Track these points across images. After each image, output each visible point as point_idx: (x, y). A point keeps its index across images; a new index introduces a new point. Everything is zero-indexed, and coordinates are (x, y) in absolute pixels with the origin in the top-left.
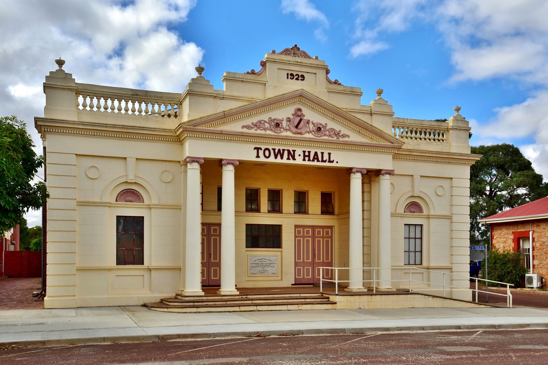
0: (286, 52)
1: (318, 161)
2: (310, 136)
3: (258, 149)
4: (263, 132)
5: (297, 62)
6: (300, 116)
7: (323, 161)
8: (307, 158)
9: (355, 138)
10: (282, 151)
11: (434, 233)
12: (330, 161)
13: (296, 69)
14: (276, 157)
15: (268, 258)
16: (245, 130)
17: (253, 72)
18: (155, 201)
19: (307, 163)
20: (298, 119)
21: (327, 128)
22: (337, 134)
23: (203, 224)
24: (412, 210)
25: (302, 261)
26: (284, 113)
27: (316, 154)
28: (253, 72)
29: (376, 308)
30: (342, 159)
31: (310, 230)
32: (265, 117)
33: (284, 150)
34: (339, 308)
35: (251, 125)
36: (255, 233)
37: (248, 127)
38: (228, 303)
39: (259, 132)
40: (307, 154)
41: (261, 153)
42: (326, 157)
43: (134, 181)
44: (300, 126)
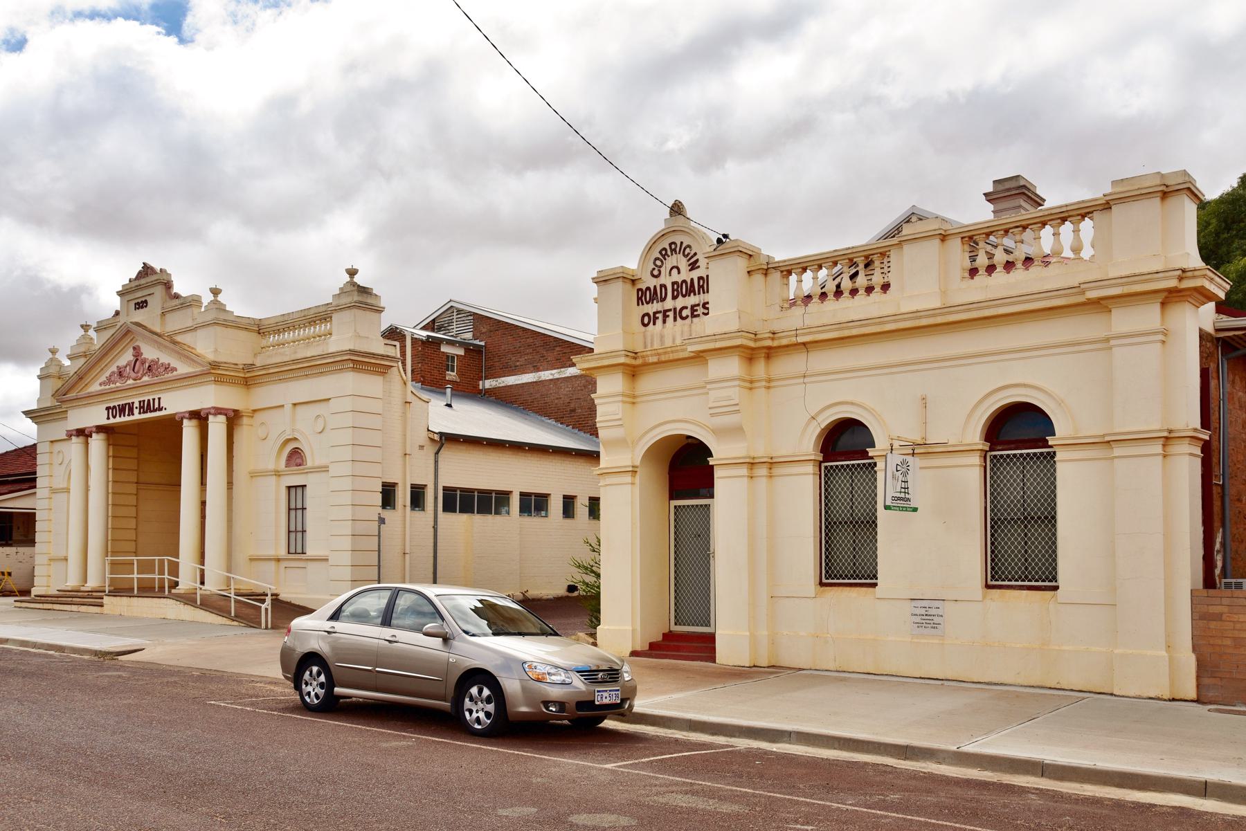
30: (175, 403)
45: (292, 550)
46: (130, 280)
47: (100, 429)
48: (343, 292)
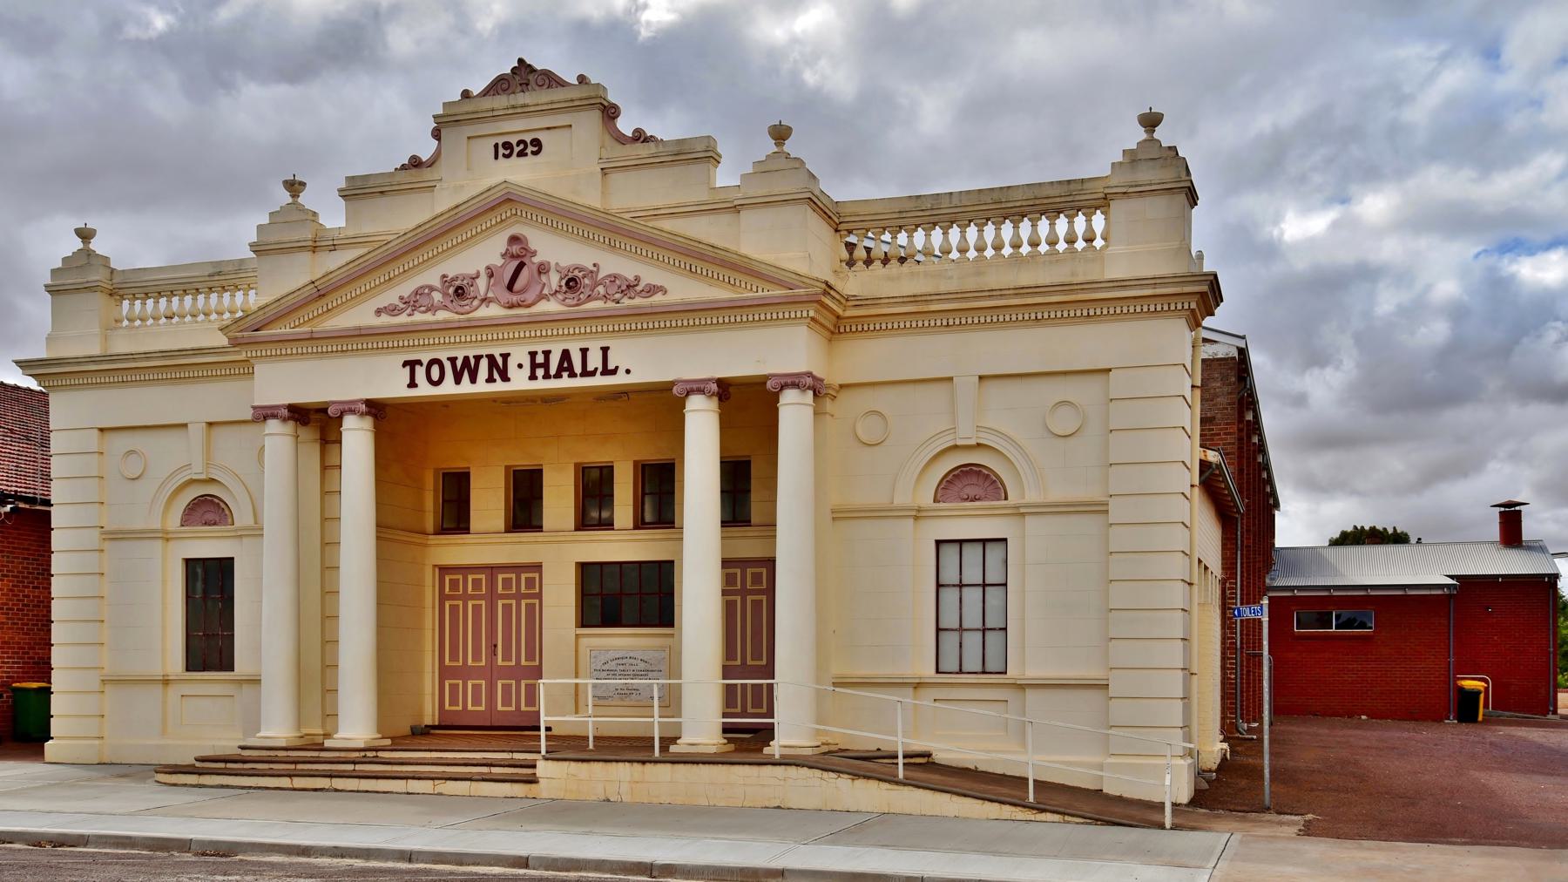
0: (499, 85)
1: (572, 375)
2: (551, 307)
3: (412, 365)
4: (428, 317)
5: (514, 107)
6: (518, 256)
7: (586, 373)
8: (540, 372)
9: (682, 289)
10: (472, 361)
11: (1038, 560)
12: (606, 372)
13: (515, 128)
14: (458, 380)
15: (639, 655)
16: (385, 320)
17: (415, 163)
18: (1032, 497)
19: (541, 384)
20: (516, 263)
21: (601, 276)
22: (630, 288)
23: (726, 563)
24: (971, 491)
25: (738, 662)
26: (481, 256)
27: (566, 355)
28: (415, 163)
29: (655, 800)
30: (642, 361)
31: (483, 577)
32: (432, 277)
33: (478, 358)
34: (544, 795)
35: (397, 302)
36: (612, 585)
37: (392, 310)
38: (300, 767)
39: (418, 317)
40: (540, 359)
41: (420, 372)
42: (595, 361)
43: (973, 442)
44: (517, 286)
45: (950, 663)
46: (466, 94)
47: (376, 409)
48: (1132, 158)
